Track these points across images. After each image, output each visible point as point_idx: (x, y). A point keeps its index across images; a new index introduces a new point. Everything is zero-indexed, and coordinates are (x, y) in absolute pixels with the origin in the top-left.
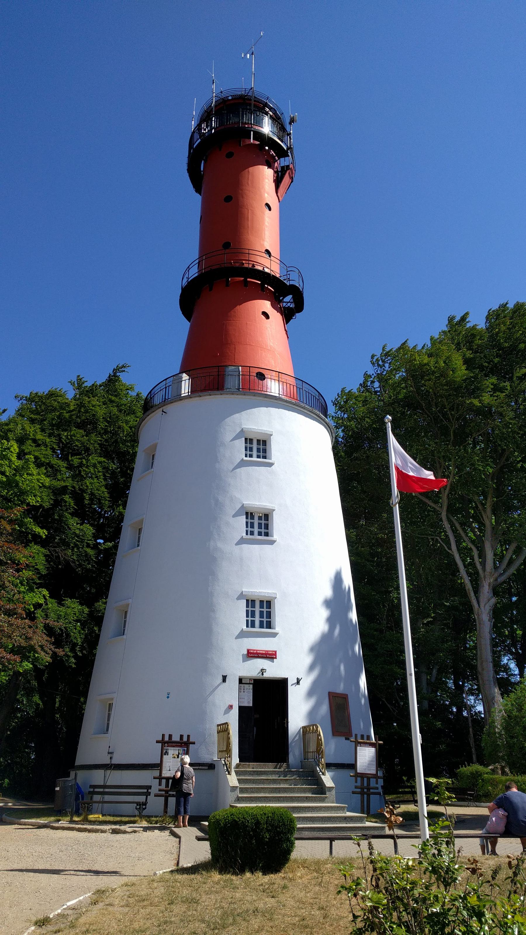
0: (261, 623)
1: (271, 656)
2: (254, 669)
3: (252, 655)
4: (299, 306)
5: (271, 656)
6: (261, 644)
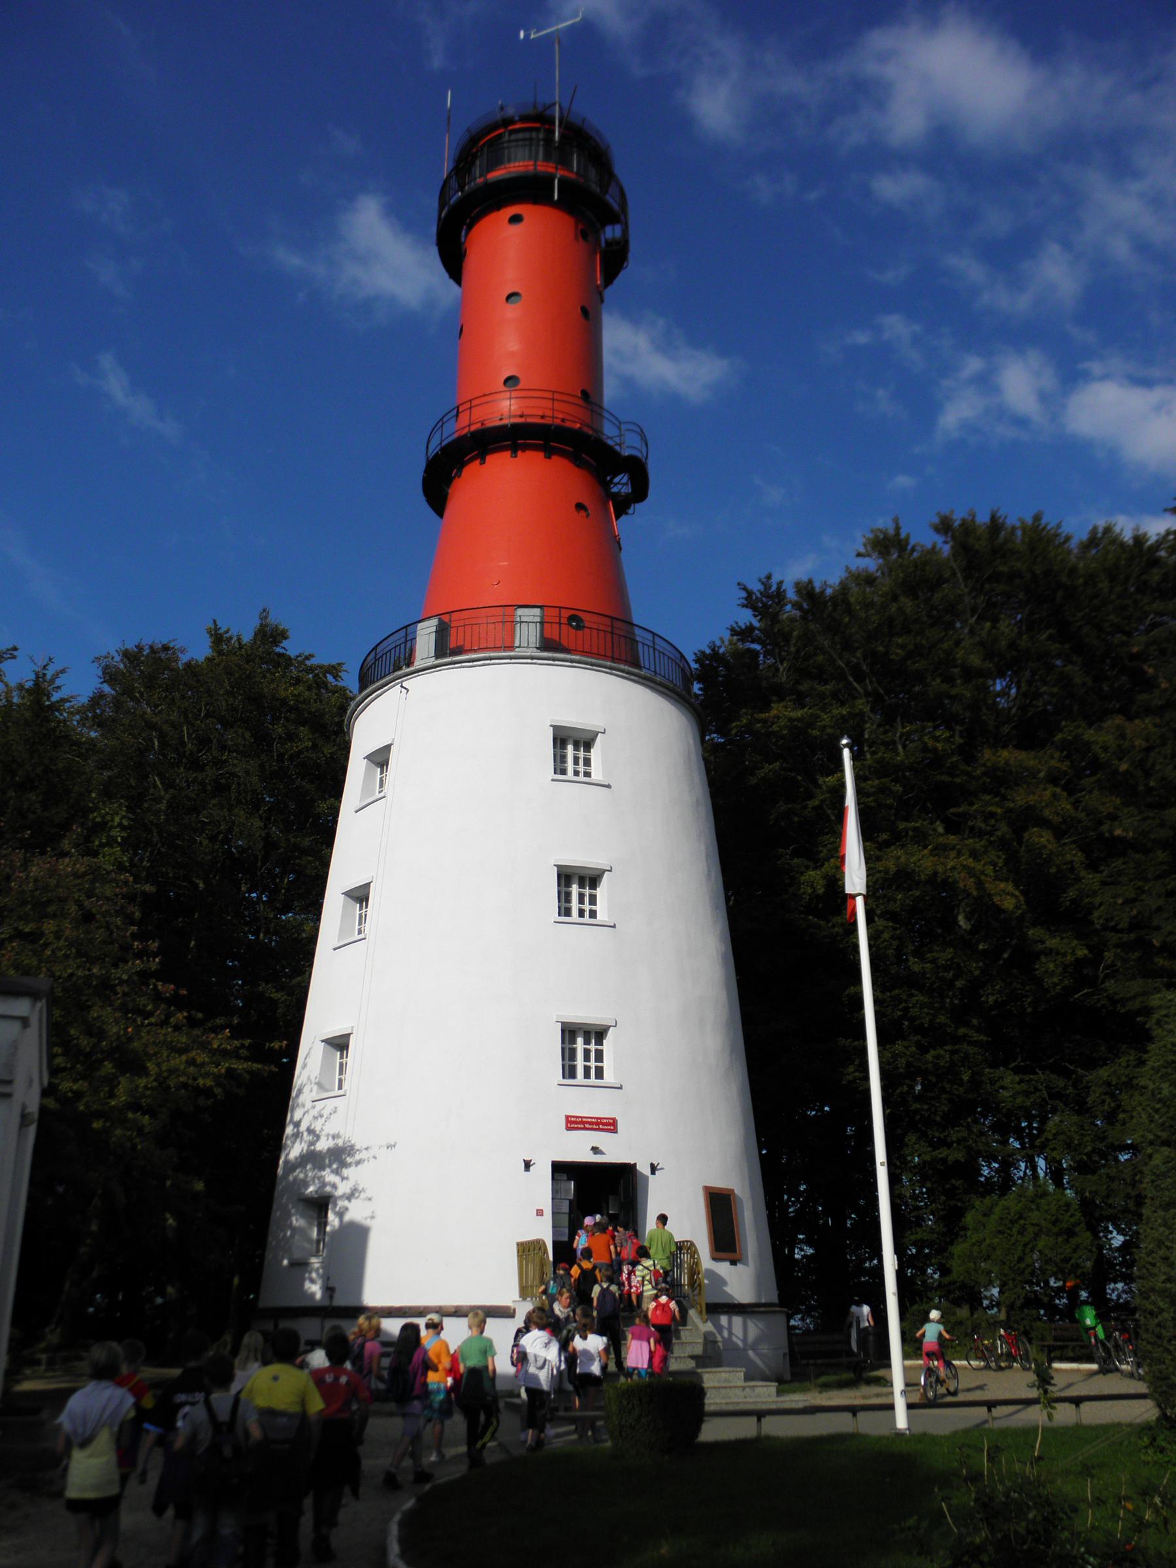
0: (587, 1070)
1: (610, 1126)
2: (578, 1148)
3: (574, 1123)
4: (640, 491)
5: (610, 1126)
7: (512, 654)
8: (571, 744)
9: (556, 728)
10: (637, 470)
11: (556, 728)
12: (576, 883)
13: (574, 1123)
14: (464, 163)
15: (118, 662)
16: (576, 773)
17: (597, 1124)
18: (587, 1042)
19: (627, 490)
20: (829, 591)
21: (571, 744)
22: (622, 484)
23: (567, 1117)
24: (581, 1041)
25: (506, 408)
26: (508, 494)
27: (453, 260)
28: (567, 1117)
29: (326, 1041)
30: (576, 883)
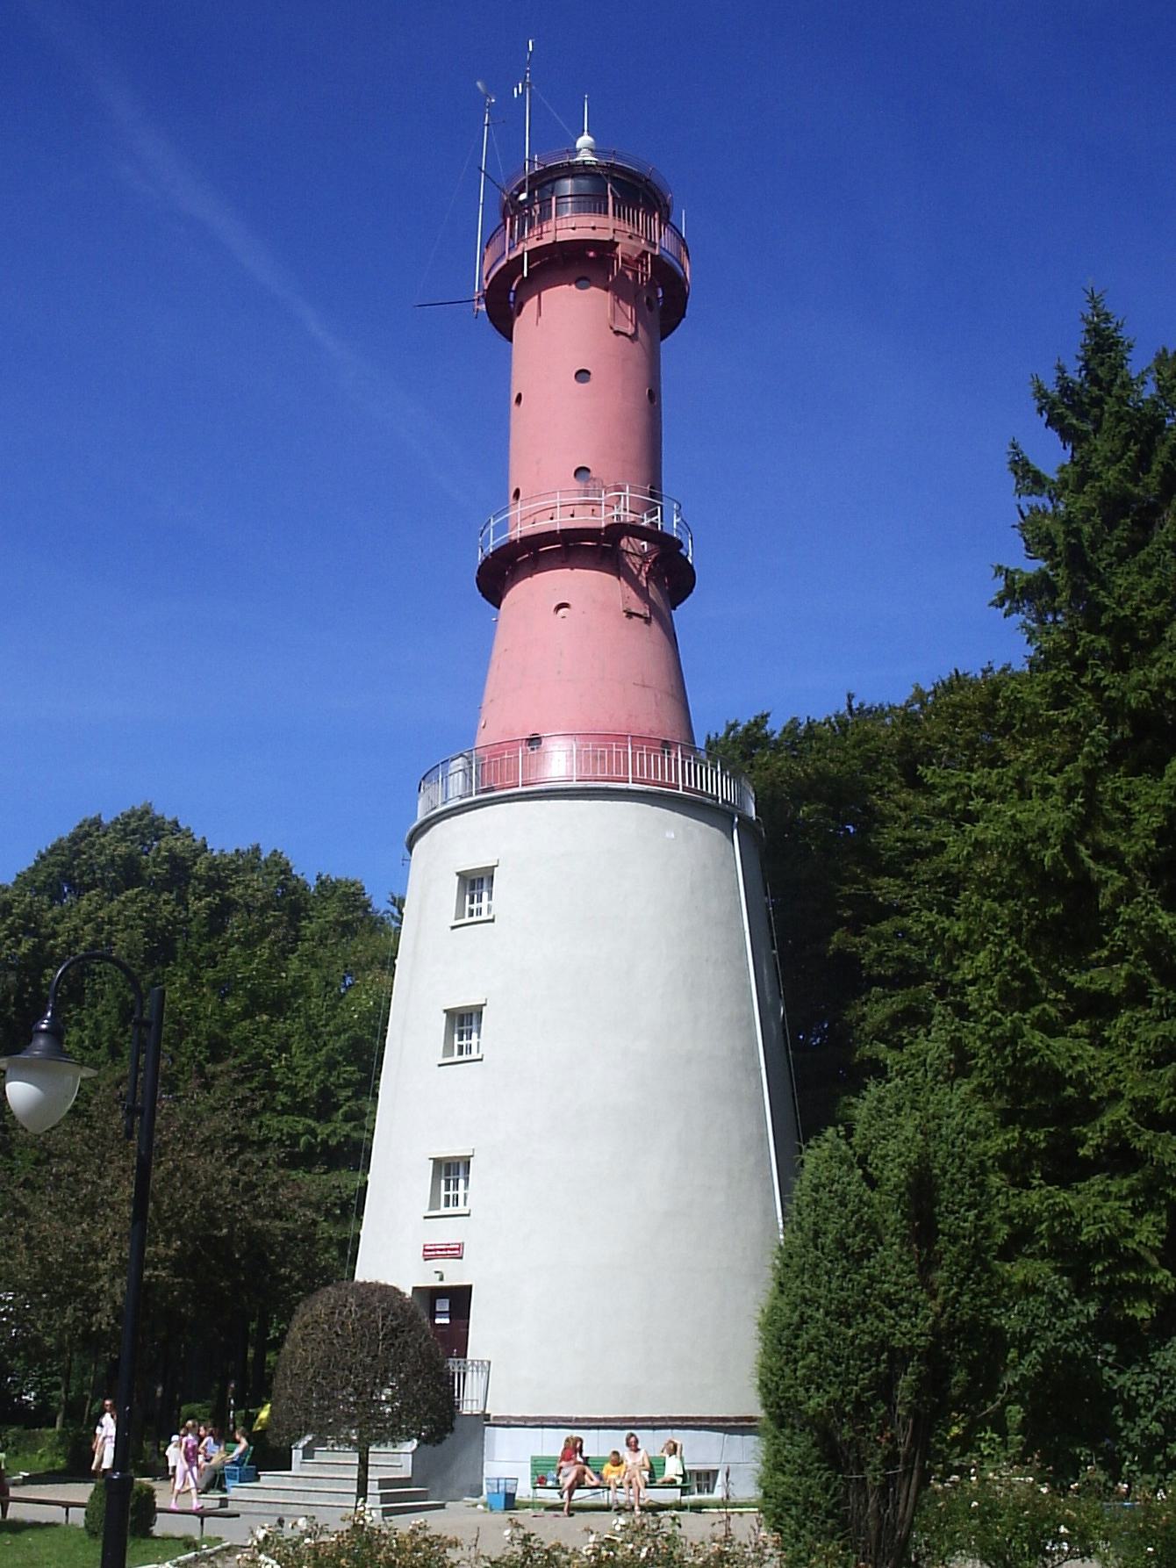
1: (455, 1252)
3: (430, 1253)
5: (455, 1252)
13: (430, 1253)
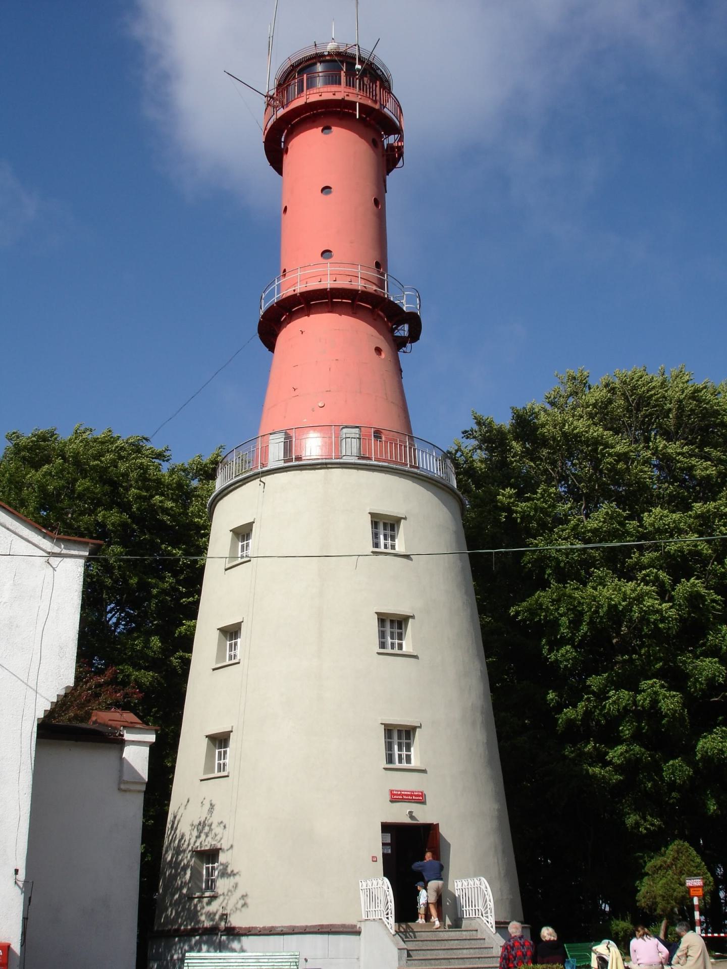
1: (419, 798)
2: (400, 814)
3: (396, 797)
4: (415, 335)
5: (419, 798)
6: (406, 783)
7: (341, 461)
8: (385, 525)
9: (373, 515)
10: (414, 321)
11: (373, 515)
12: (392, 625)
13: (396, 797)
14: (283, 84)
15: (505, 421)
16: (386, 547)
17: (411, 795)
18: (392, 627)
19: (406, 334)
20: (638, 904)
21: (385, 525)
22: (404, 330)
23: (391, 791)
24: (399, 736)
25: (326, 277)
26: (319, 340)
27: (275, 152)
28: (391, 791)
29: (220, 630)
30: (392, 625)
